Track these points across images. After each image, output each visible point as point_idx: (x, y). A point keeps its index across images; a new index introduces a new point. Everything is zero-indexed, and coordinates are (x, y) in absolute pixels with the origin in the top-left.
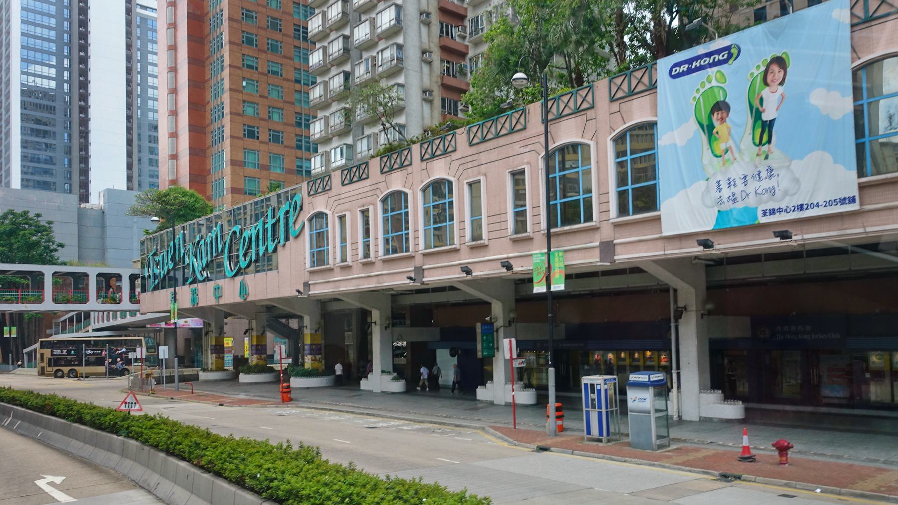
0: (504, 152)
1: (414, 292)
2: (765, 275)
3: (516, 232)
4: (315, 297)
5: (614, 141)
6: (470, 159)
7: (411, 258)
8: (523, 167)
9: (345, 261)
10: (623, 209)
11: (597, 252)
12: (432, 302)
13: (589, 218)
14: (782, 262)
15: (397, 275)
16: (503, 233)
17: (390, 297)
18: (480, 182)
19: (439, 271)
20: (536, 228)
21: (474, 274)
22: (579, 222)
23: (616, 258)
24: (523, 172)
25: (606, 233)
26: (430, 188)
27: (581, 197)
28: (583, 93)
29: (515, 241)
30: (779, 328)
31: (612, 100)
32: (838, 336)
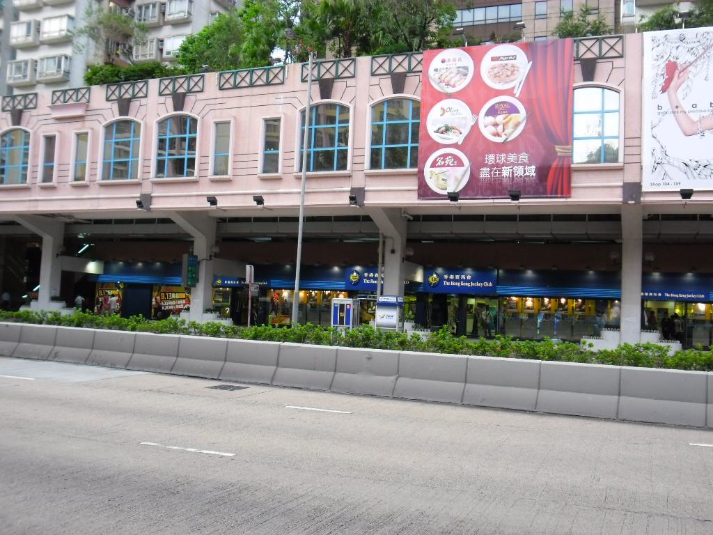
0: (264, 100)
1: (92, 222)
2: (362, 231)
3: (44, 181)
4: (225, 210)
5: (372, 107)
6: (219, 101)
7: (139, 184)
8: (279, 116)
9: (82, 178)
10: (375, 163)
11: (619, 192)
12: (114, 233)
13: (343, 166)
14: (534, 223)
15: (587, 190)
16: (251, 171)
17: (63, 226)
18: (229, 123)
19: (182, 199)
20: (289, 170)
21: (218, 205)
22: (333, 170)
23: (151, 207)
24: (278, 120)
25: (358, 182)
26: (115, 126)
27: (336, 148)
28: (346, 64)
29: (102, 186)
30: (446, 277)
31: (373, 74)
32: (491, 285)
